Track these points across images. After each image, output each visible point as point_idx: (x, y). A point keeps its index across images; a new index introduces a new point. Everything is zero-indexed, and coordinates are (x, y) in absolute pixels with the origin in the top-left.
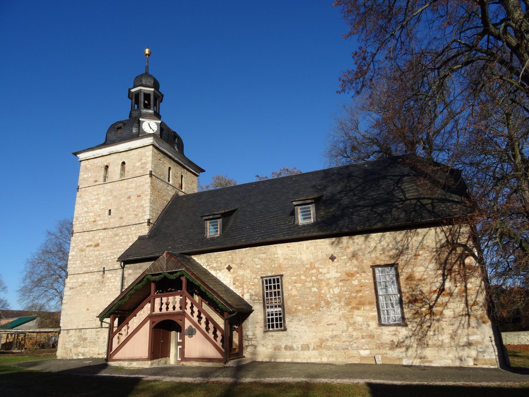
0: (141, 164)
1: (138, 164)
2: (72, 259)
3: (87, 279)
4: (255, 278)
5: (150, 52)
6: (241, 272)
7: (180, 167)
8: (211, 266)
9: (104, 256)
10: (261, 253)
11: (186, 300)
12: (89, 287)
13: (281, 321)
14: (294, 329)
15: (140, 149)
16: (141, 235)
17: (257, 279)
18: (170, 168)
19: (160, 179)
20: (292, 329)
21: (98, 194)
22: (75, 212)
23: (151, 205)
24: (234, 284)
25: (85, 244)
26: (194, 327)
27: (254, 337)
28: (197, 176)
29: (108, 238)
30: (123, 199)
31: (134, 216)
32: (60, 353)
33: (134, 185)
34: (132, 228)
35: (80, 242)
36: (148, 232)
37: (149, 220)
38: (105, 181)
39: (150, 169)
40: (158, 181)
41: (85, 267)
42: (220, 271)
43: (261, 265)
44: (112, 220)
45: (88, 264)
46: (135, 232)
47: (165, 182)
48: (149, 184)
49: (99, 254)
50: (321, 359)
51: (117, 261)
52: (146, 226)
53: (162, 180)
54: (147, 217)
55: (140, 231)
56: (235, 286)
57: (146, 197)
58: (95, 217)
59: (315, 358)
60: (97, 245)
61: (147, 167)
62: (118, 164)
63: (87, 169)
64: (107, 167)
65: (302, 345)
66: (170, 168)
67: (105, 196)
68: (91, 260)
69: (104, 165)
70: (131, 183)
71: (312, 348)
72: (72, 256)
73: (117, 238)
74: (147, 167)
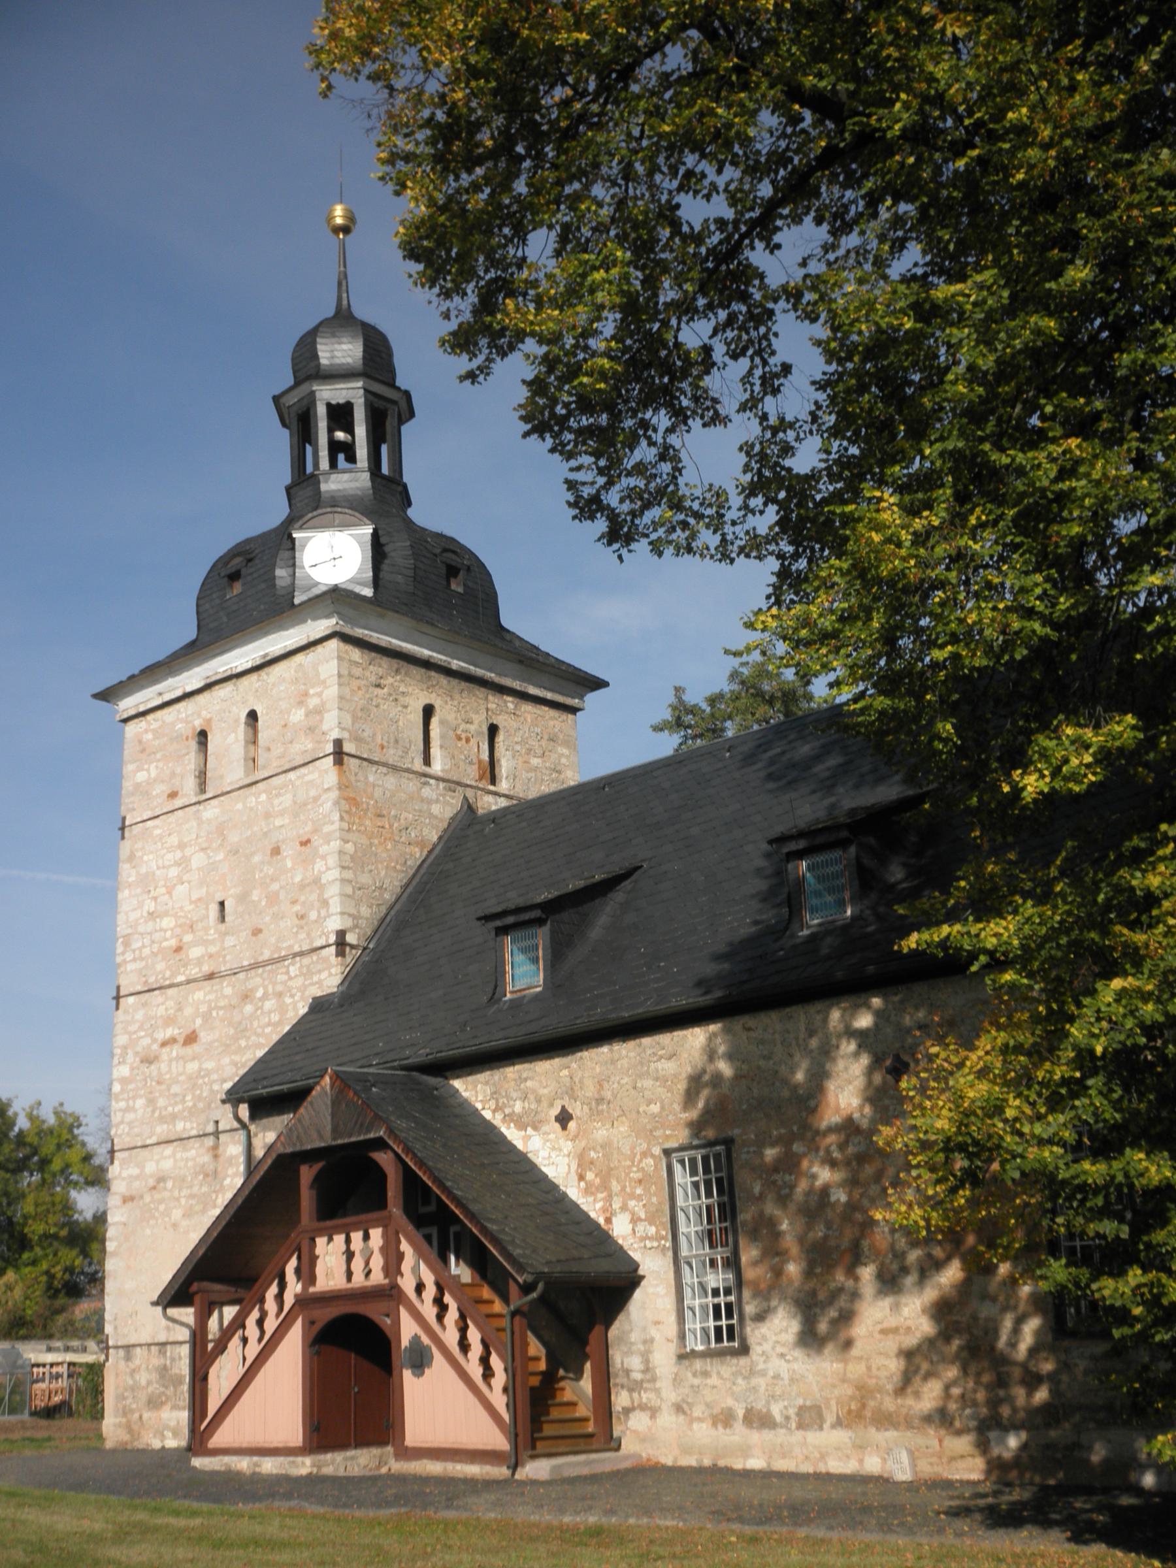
0: (307, 715)
1: (297, 716)
2: (123, 1090)
3: (167, 1165)
4: (644, 1155)
5: (350, 217)
6: (601, 1133)
7: (481, 692)
8: (507, 1111)
9: (215, 1077)
10: (661, 1057)
11: (399, 1242)
12: (176, 1194)
13: (729, 1315)
14: (773, 1348)
15: (299, 658)
16: (319, 994)
17: (653, 1156)
18: (428, 711)
19: (385, 765)
20: (767, 1347)
21: (182, 846)
22: (121, 918)
23: (349, 875)
24: (581, 1178)
25: (156, 1035)
26: (426, 1340)
27: (648, 1376)
28: (573, 710)
29: (221, 1008)
30: (256, 859)
31: (296, 921)
32: (112, 1427)
33: (286, 800)
34: (291, 968)
35: (141, 1028)
36: (337, 980)
37: (341, 934)
38: (203, 791)
39: (335, 734)
40: (373, 775)
41: (162, 1119)
42: (535, 1128)
43: (662, 1102)
44: (230, 941)
45: (170, 1109)
46: (299, 982)
47: (408, 771)
48: (334, 794)
49: (200, 1070)
50: (861, 1461)
51: (224, 1102)
52: (333, 959)
53: (395, 769)
54: (335, 923)
55: (315, 979)
56: (582, 1184)
57: (328, 843)
58: (178, 931)
59: (840, 1459)
60: (191, 1039)
61: (325, 727)
62: (237, 721)
63: (143, 751)
64: (203, 736)
65: (801, 1408)
66: (428, 711)
67: (203, 850)
68: (176, 1095)
69: (194, 728)
70: (278, 795)
71: (830, 1419)
72: (124, 1081)
73: (248, 1008)
74: (325, 727)
